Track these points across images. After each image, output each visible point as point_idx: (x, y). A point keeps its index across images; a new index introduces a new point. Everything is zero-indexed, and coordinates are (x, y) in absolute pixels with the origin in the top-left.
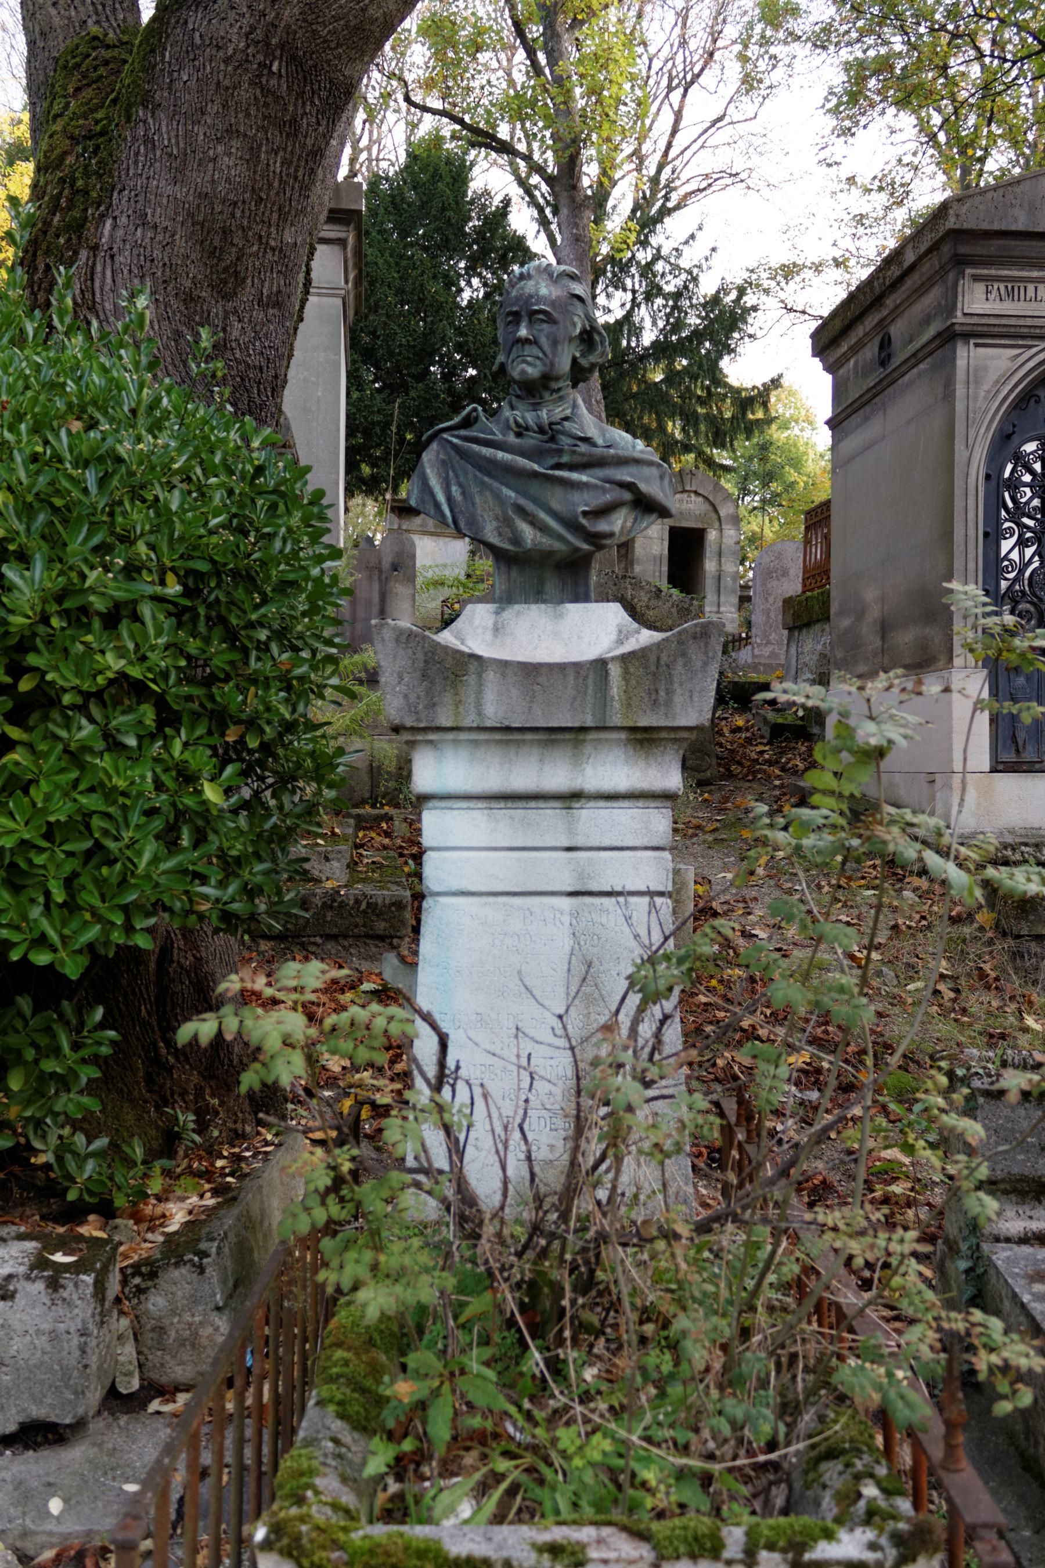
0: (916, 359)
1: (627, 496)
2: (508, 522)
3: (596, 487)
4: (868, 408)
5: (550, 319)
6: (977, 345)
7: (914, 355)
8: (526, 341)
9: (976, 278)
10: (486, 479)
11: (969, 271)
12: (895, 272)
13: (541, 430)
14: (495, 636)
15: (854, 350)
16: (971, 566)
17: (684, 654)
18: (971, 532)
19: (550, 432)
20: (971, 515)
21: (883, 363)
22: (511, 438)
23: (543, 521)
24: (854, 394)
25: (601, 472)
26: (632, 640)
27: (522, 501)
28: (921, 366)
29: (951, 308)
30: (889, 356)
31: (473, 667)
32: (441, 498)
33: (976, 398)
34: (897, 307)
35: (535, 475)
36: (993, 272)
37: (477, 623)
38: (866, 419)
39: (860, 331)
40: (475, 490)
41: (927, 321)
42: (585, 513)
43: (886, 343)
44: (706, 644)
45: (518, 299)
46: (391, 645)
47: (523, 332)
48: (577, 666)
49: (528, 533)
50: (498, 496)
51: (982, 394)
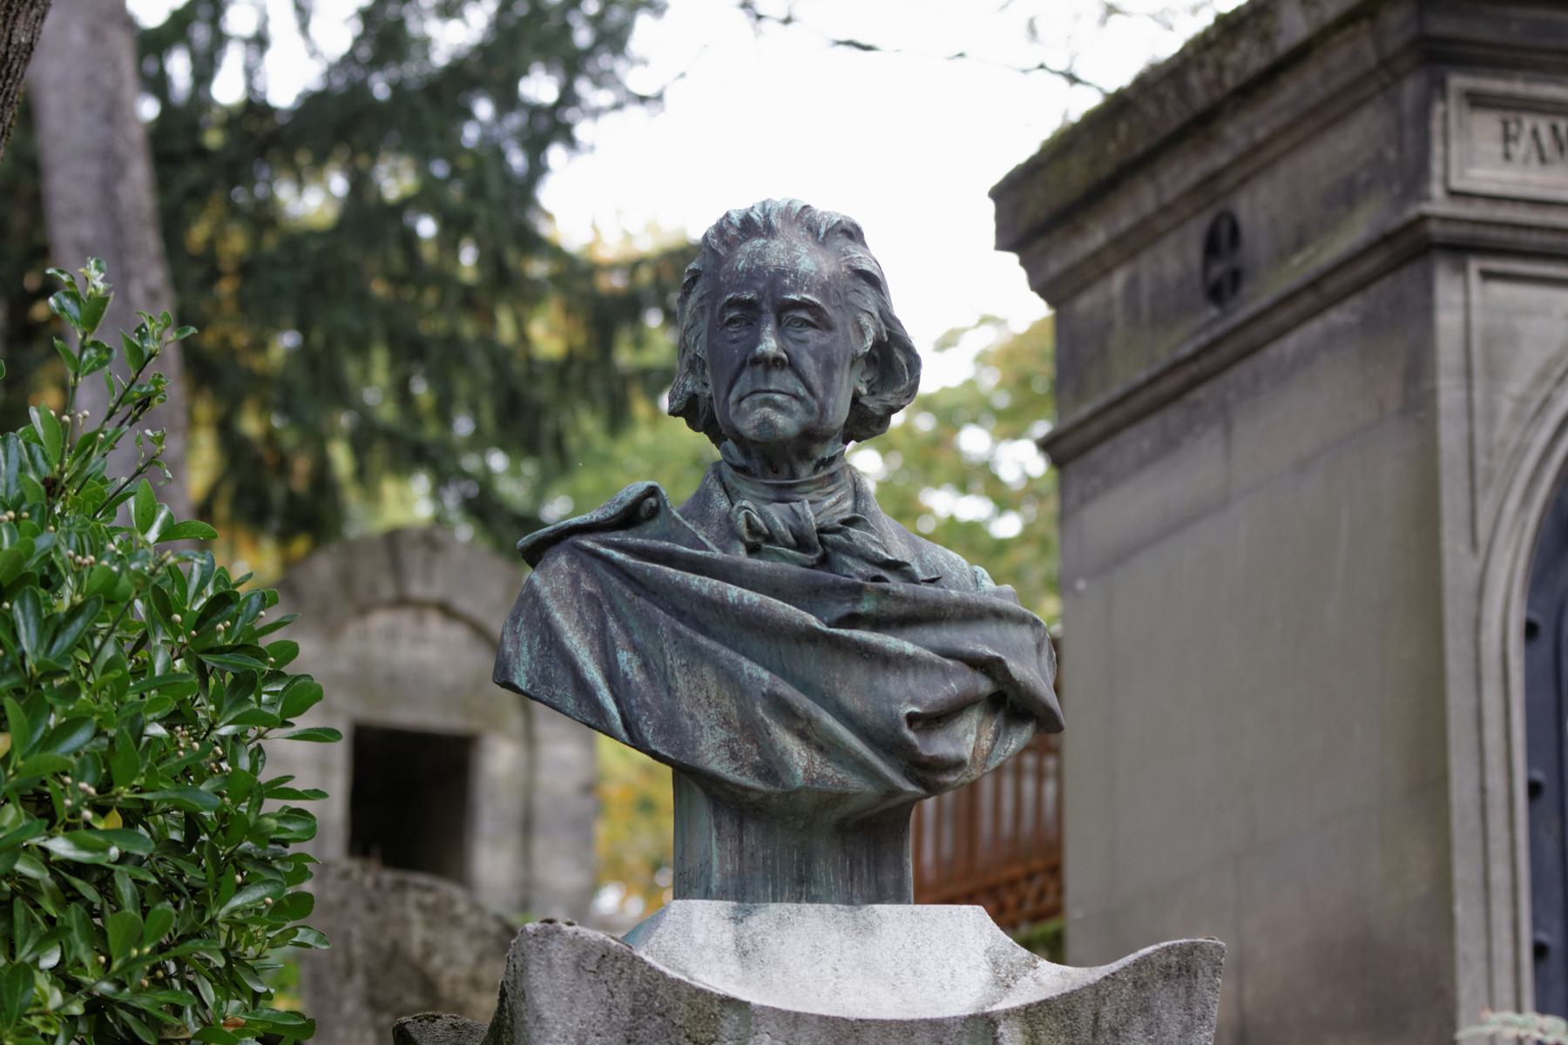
0: (1317, 294)
1: (985, 686)
2: (752, 731)
3: (931, 665)
4: (1174, 416)
5: (819, 319)
6: (1487, 275)
7: (1314, 284)
8: (773, 363)
9: (1477, 101)
10: (702, 640)
11: (1458, 82)
12: (1249, 57)
13: (802, 543)
14: (745, 967)
15: (1126, 247)
16: (1500, 874)
17: (1145, 1010)
18: (1496, 781)
19: (821, 547)
20: (1493, 735)
21: (1218, 293)
22: (740, 554)
23: (829, 731)
24: (1128, 369)
25: (950, 636)
26: (1026, 980)
27: (786, 690)
28: (1337, 317)
29: (1415, 177)
30: (1236, 277)
31: (729, 1024)
32: (593, 673)
33: (1492, 416)
34: (1257, 148)
35: (812, 636)
36: (1518, 87)
37: (700, 938)
38: (1170, 444)
39: (1143, 199)
40: (674, 661)
41: (1347, 195)
42: (912, 719)
43: (1222, 240)
44: (1189, 990)
45: (752, 276)
46: (565, 975)
47: (770, 345)
48: (935, 1025)
49: (798, 757)
50: (730, 677)
51: (1506, 407)
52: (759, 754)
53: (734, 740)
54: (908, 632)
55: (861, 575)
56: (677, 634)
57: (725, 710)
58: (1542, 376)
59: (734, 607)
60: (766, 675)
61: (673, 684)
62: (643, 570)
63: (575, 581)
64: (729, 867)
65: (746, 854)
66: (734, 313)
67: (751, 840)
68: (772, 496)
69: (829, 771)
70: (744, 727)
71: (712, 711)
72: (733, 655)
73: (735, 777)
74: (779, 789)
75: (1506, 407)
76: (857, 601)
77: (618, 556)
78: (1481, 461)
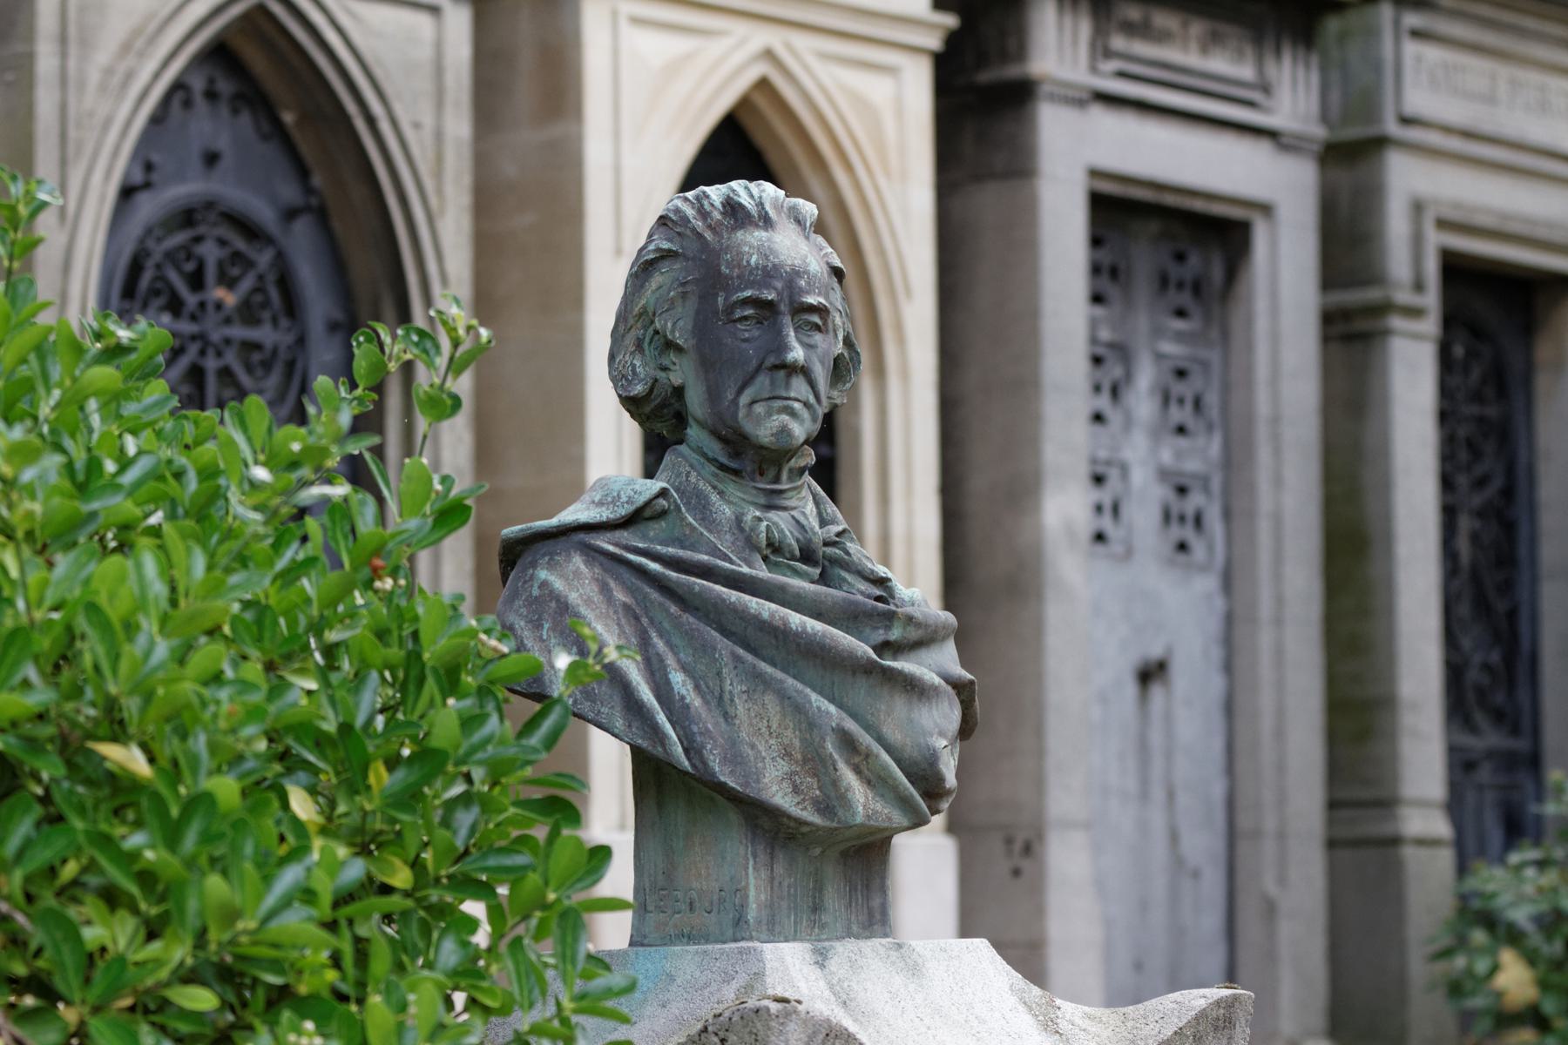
23: (885, 768)
27: (851, 725)
32: (646, 694)
33: (82, 85)
40: (734, 686)
50: (796, 709)
51: (94, 77)
52: (819, 788)
53: (796, 773)
54: (913, 655)
55: (862, 593)
56: (737, 659)
57: (786, 741)
58: (126, 48)
59: (797, 634)
60: (832, 709)
61: (731, 711)
62: (690, 587)
63: (605, 589)
64: (763, 897)
65: (776, 883)
66: (749, 312)
67: (779, 869)
68: (762, 501)
69: (879, 807)
70: (805, 761)
71: (772, 742)
72: (800, 686)
73: (796, 811)
74: (835, 825)
75: (94, 77)
76: (888, 628)
77: (654, 566)
78: (72, 133)
